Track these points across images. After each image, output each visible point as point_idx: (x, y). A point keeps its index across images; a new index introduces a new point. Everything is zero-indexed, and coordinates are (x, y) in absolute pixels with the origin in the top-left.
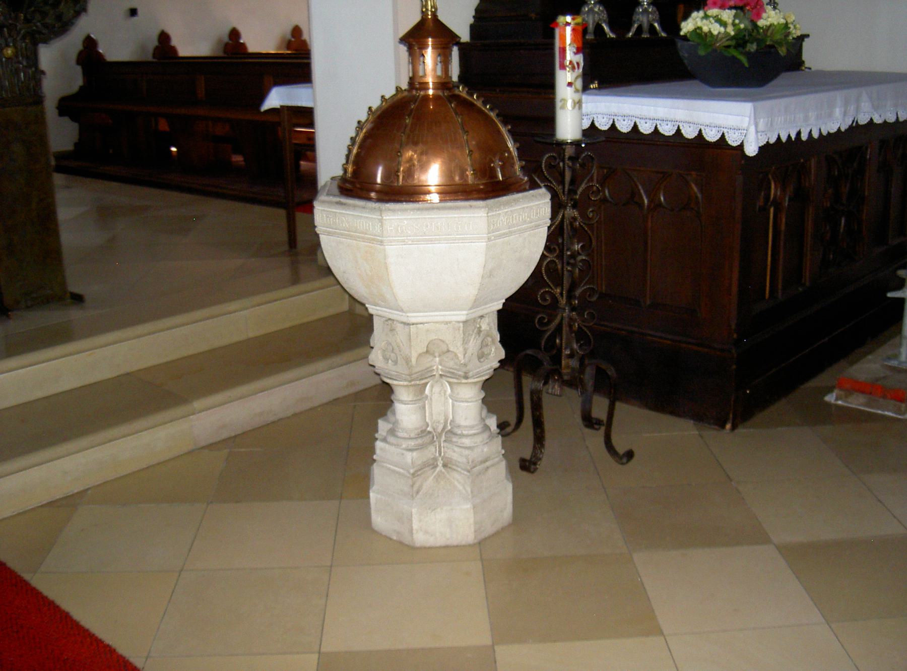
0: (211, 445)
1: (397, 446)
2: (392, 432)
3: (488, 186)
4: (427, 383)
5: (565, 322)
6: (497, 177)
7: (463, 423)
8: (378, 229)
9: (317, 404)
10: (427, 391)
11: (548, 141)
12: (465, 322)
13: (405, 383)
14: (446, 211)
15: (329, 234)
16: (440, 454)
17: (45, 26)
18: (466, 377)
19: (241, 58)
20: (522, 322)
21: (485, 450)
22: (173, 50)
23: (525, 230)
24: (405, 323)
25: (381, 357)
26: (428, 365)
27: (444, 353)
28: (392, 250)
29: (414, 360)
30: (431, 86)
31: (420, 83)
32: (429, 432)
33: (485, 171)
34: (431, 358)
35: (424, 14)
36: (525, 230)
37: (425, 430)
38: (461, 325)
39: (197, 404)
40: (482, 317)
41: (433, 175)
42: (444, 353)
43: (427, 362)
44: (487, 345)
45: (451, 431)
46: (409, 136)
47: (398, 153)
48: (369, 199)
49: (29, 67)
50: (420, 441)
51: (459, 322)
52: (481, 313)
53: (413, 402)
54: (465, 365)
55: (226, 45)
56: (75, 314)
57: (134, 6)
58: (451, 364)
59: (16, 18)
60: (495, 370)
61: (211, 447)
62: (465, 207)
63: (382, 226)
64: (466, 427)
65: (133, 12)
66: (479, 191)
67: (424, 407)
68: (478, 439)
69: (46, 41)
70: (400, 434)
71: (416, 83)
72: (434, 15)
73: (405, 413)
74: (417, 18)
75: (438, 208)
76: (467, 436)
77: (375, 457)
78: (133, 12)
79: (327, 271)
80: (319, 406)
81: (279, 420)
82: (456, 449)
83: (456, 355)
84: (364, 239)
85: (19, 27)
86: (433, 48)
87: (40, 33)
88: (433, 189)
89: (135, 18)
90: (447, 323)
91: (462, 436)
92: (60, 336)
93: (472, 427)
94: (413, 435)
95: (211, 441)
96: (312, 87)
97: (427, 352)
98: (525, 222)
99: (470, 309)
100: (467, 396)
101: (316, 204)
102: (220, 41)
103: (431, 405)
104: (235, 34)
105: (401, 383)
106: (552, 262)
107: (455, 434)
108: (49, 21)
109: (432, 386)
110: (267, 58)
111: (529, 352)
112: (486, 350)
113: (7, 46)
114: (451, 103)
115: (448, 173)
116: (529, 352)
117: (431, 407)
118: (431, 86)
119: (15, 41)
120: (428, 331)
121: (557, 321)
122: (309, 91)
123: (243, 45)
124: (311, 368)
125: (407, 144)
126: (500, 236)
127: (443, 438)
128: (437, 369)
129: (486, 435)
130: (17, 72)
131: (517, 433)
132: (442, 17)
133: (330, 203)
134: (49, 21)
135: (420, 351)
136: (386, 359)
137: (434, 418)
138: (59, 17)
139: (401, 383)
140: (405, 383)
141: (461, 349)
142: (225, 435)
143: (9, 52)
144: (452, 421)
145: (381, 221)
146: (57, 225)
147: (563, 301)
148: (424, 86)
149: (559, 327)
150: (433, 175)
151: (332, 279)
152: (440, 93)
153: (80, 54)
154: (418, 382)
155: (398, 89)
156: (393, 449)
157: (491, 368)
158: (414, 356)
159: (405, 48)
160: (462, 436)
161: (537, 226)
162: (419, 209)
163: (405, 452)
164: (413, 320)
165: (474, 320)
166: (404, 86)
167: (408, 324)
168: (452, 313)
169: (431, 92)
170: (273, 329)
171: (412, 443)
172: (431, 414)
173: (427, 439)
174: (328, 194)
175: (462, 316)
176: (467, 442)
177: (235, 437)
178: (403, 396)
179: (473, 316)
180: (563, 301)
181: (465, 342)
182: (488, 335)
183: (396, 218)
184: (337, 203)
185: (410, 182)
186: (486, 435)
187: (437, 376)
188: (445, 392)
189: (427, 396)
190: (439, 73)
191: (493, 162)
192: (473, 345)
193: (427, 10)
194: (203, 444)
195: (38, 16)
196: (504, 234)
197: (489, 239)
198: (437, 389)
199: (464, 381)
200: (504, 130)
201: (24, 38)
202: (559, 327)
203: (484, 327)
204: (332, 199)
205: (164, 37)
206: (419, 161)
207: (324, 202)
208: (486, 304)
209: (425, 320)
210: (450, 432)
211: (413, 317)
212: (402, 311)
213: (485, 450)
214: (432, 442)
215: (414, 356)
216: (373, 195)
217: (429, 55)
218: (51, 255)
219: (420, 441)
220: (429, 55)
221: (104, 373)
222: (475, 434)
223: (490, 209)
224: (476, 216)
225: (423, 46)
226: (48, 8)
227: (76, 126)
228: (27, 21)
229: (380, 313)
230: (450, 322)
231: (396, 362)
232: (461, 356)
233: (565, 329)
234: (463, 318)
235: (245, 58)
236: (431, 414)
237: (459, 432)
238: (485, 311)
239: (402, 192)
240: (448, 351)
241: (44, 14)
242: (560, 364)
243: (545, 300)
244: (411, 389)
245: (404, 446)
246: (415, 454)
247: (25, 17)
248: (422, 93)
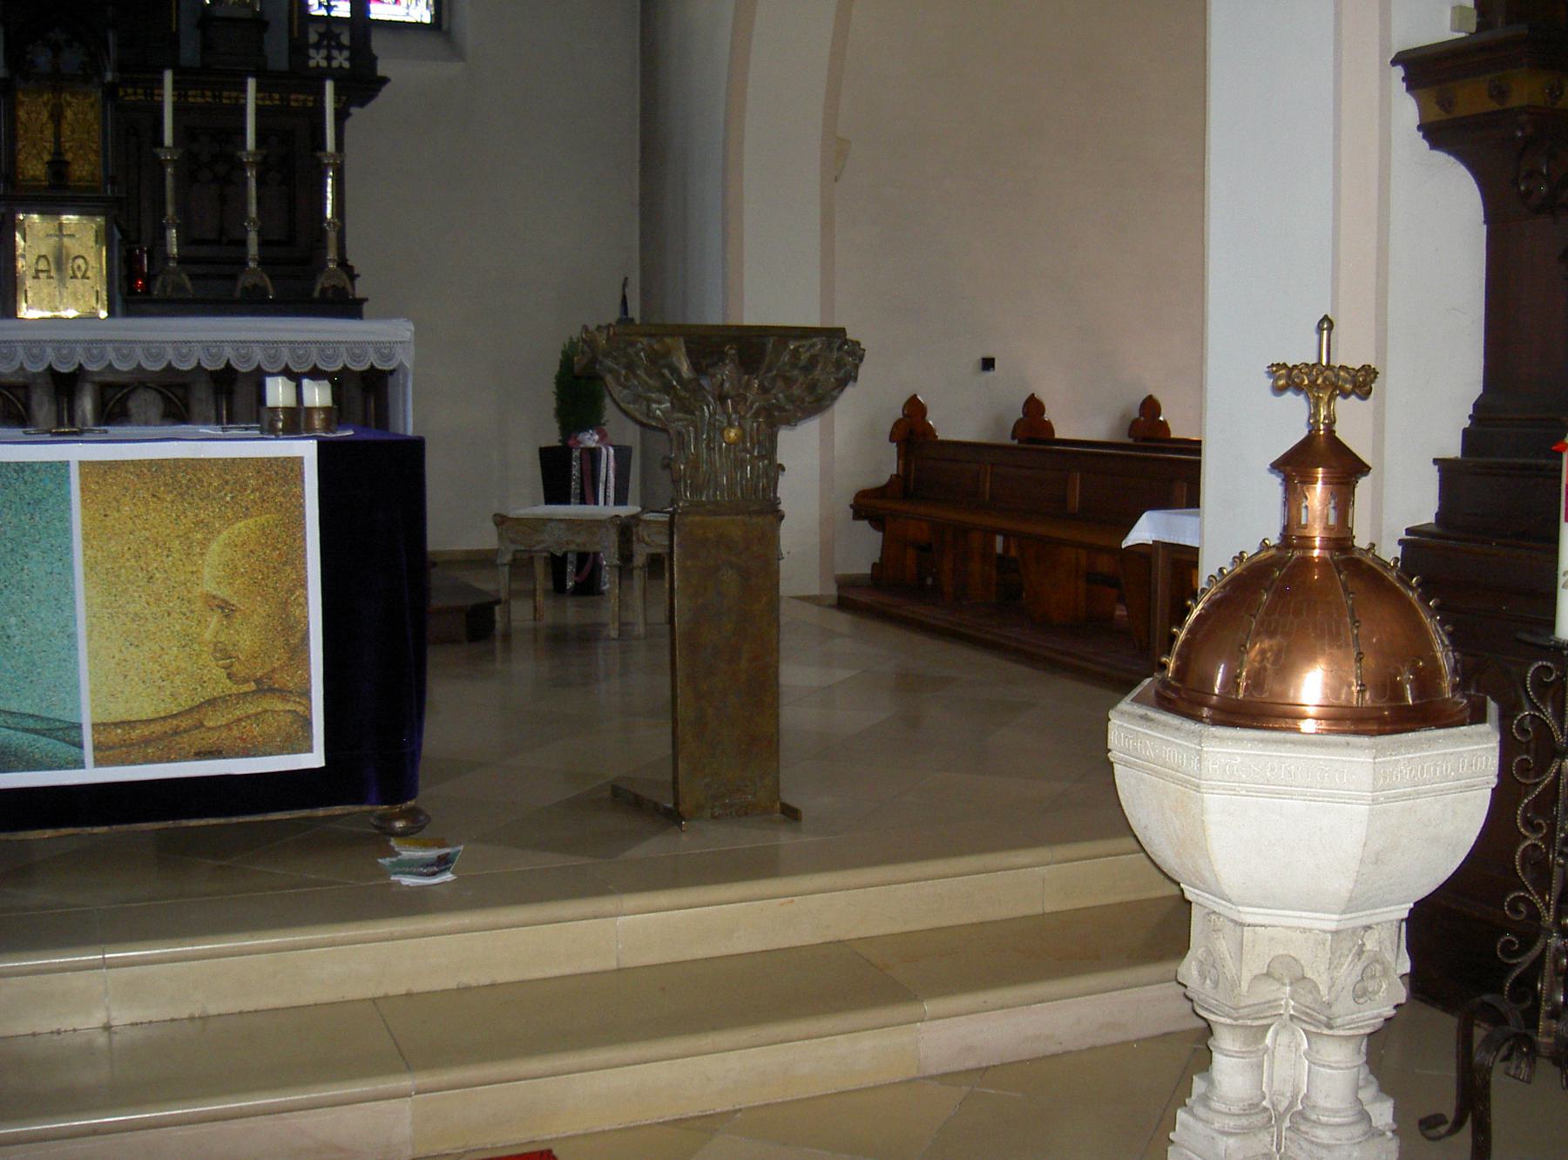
0: (946, 1074)
1: (1206, 1122)
2: (1205, 1100)
3: (1391, 710)
4: (1269, 1026)
5: (1549, 956)
6: (1404, 698)
7: (1321, 1103)
8: (1194, 765)
9: (1133, 1037)
10: (1268, 1040)
11: (1541, 641)
12: (1336, 933)
13: (1229, 1021)
14: (1305, 749)
15: (1126, 764)
16: (1278, 1150)
17: (790, 399)
18: (1330, 1027)
19: (1156, 450)
20: (1460, 943)
21: (1355, 1154)
22: (1049, 427)
23: (1444, 792)
24: (1236, 922)
25: (1195, 973)
26: (1271, 997)
27: (1298, 980)
28: (1214, 802)
29: (1245, 985)
30: (1317, 543)
31: (1300, 538)
32: (1266, 1109)
33: (1389, 690)
34: (1276, 986)
35: (1313, 429)
36: (1444, 792)
37: (1257, 1105)
38: (1329, 937)
39: (929, 1007)
40: (1368, 928)
41: (1312, 686)
42: (1298, 980)
43: (1268, 990)
44: (1373, 977)
45: (1301, 1114)
46: (1262, 624)
47: (1241, 649)
48: (1198, 719)
49: (761, 457)
50: (1244, 1121)
51: (1324, 931)
52: (1366, 922)
53: (1240, 1055)
54: (1329, 1005)
55: (1135, 423)
56: (785, 838)
57: (989, 354)
58: (1308, 1000)
59: (748, 386)
60: (1387, 1020)
61: (945, 1078)
62: (1336, 745)
63: (1200, 761)
64: (1325, 1109)
65: (988, 364)
66: (1381, 720)
67: (1260, 1066)
68: (1344, 1133)
69: (791, 421)
70: (1215, 1105)
71: (1292, 536)
72: (1330, 431)
73: (1230, 1072)
74: (1303, 433)
75: (1314, 744)
76: (1326, 1125)
77: (1172, 1136)
78: (988, 364)
79: (1121, 826)
80: (1137, 1041)
81: (1065, 1053)
82: (1305, 1145)
83: (1316, 986)
84: (1176, 781)
85: (750, 397)
86: (1325, 483)
87: (781, 409)
88: (1312, 711)
89: (990, 374)
90: (1304, 930)
91: (1317, 1123)
92: (761, 866)
93: (1335, 1112)
94: (1234, 1109)
95: (946, 1069)
96: (1198, 515)
97: (1268, 975)
98: (1445, 778)
99: (1344, 912)
100: (1333, 1059)
101: (1112, 714)
102: (1123, 417)
103: (1272, 1063)
104: (1150, 406)
105: (1222, 1020)
106: (1535, 846)
107: (1306, 1119)
108: (796, 391)
109: (1276, 1034)
110: (1180, 451)
111: (1487, 998)
112: (1371, 985)
113: (730, 425)
114: (1340, 573)
115: (1334, 688)
116: (1487, 998)
117: (1271, 1067)
118: (1317, 543)
119: (742, 417)
120: (1272, 939)
121: (1539, 947)
122: (1194, 519)
123: (1164, 424)
124: (1127, 975)
125: (1258, 634)
126: (1396, 798)
127: (1287, 1124)
128: (1287, 1004)
129: (1359, 1130)
130: (741, 464)
131: (1453, 1139)
132: (1340, 434)
133: (1132, 715)
134: (796, 391)
135: (1257, 972)
136: (1203, 976)
137: (1276, 1084)
138: (812, 387)
139: (1222, 1020)
140: (1229, 1021)
141: (1325, 977)
142: (971, 1063)
143: (732, 434)
144: (1307, 1096)
145: (1199, 753)
146: (776, 696)
147: (1549, 918)
148: (1306, 542)
149: (1539, 963)
150: (1312, 686)
151: (1132, 840)
152: (1327, 555)
153: (897, 424)
154: (1249, 1022)
155: (1264, 546)
156: (1200, 1126)
157: (1379, 1016)
158: (1246, 976)
159: (1279, 480)
160: (1317, 1123)
161: (1470, 787)
162: (1262, 741)
163: (1218, 1137)
164: (1248, 919)
165: (1354, 930)
166: (1274, 540)
167: (1242, 925)
168: (1299, 913)
169: (1316, 553)
170: (1089, 902)
171: (1230, 1123)
172: (1271, 1079)
173: (1257, 1120)
174: (1135, 700)
175: (1330, 922)
176: (1323, 1135)
177: (987, 1068)
178: (1226, 1044)
179: (1350, 924)
180: (1549, 918)
181: (1332, 966)
182: (1376, 959)
183: (1228, 754)
184: (1142, 717)
185: (1257, 697)
186: (1359, 1130)
187: (1286, 1017)
188: (1298, 1045)
189: (1267, 1048)
190: (1332, 521)
191: (1400, 674)
192: (1348, 972)
193: (1317, 421)
194: (933, 1071)
195: (780, 383)
196: (1404, 794)
197: (1375, 801)
198: (1284, 1038)
199: (1326, 1031)
200: (1431, 623)
201: (756, 415)
202: (1539, 963)
203: (1370, 945)
204: (1142, 710)
205: (1034, 406)
206: (1275, 662)
207: (1123, 713)
208: (1375, 907)
209: (1266, 921)
210: (1300, 1116)
211: (1248, 915)
212: (1230, 901)
213: (1355, 1154)
214: (1267, 1126)
215: (1246, 976)
216: (1206, 712)
217: (1317, 495)
218: (760, 740)
219: (1244, 1121)
220: (1317, 495)
221: (745, 942)
222: (1340, 1125)
223: (1380, 751)
224: (1360, 762)
225: (1309, 480)
226: (796, 372)
227: (876, 538)
228: (764, 390)
229: (1200, 900)
230: (1310, 930)
231: (1216, 984)
232: (1323, 989)
233: (1549, 966)
234: (1333, 926)
235: (1164, 450)
236: (1271, 1079)
237: (1314, 1117)
238: (1375, 919)
239: (1258, 712)
240: (1304, 978)
241: (789, 382)
242: (1536, 1026)
243: (1519, 912)
244: (1239, 1031)
245: (1217, 1125)
246: (1232, 1141)
247: (761, 386)
248: (1297, 554)
